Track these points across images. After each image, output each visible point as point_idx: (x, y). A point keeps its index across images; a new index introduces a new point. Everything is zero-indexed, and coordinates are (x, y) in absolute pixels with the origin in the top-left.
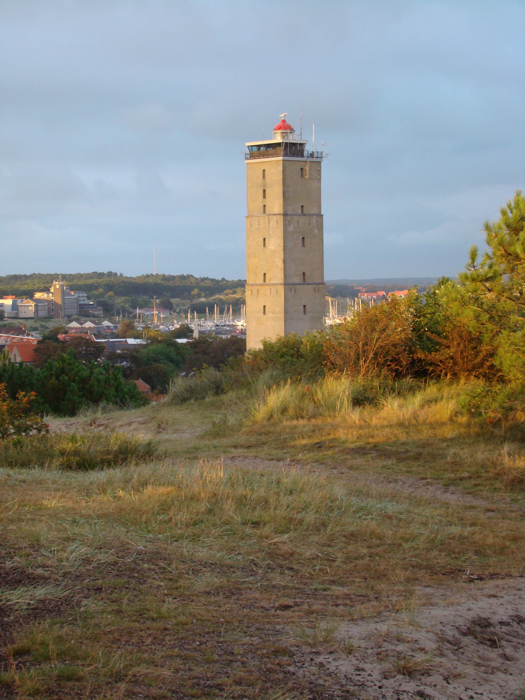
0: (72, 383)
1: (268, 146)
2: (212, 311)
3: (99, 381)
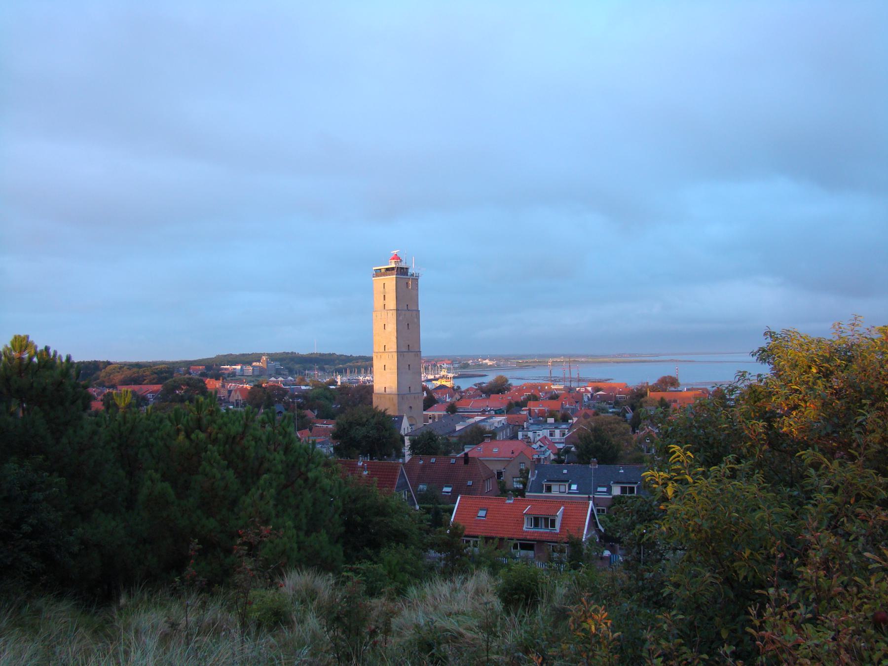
0: (210, 446)
1: (387, 269)
2: (346, 372)
3: (257, 439)
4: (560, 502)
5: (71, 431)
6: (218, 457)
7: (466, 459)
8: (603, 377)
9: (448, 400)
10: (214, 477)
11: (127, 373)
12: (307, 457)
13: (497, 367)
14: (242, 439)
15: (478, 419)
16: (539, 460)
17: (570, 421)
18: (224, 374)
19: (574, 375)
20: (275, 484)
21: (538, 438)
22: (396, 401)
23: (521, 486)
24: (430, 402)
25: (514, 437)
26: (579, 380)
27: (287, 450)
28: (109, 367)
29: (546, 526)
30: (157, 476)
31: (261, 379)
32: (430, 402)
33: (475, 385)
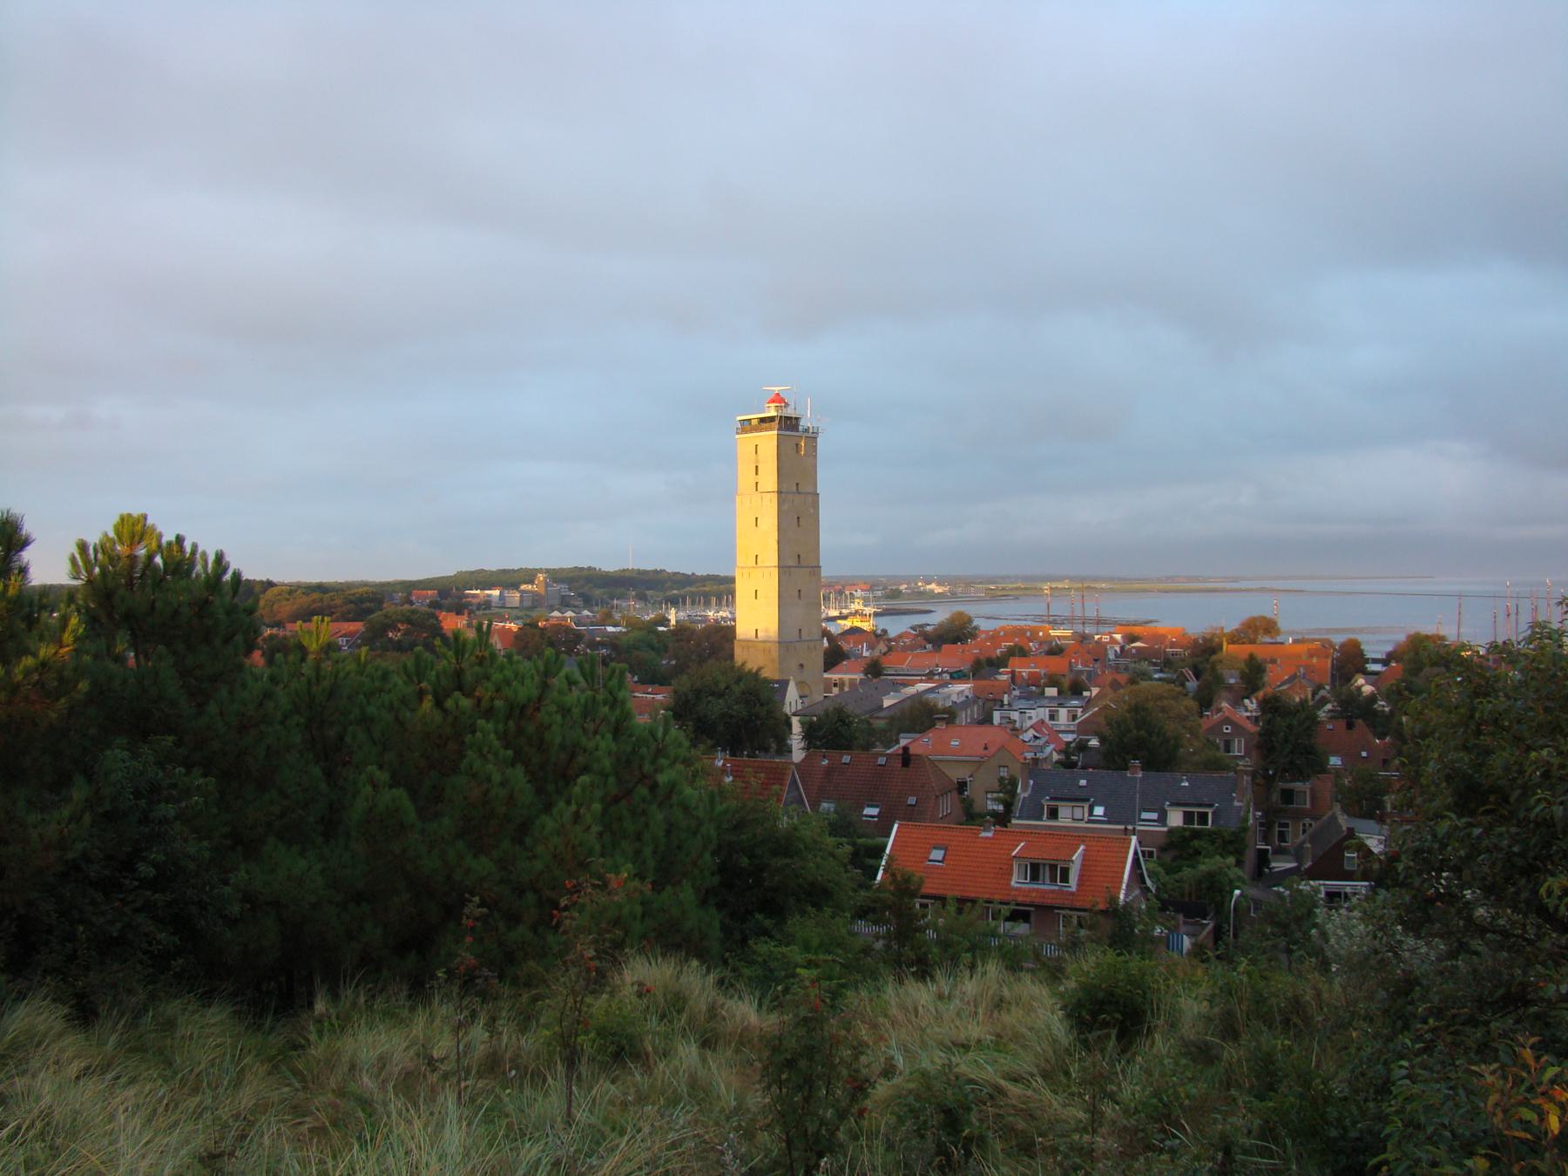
0: (481, 722)
1: (762, 420)
2: (684, 603)
3: (565, 711)
4: (1072, 837)
5: (224, 692)
6: (496, 743)
7: (906, 758)
8: (1141, 617)
9: (866, 654)
10: (489, 780)
11: (303, 601)
12: (653, 746)
13: (952, 597)
14: (538, 709)
15: (922, 687)
16: (1036, 761)
17: (1086, 694)
18: (470, 604)
19: (1091, 613)
20: (598, 793)
21: (1029, 723)
22: (775, 654)
23: (1001, 808)
24: (834, 657)
25: (987, 720)
26: (1099, 622)
27: (618, 731)
28: (271, 593)
29: (1053, 880)
30: (383, 777)
31: (534, 614)
32: (834, 657)
33: (913, 628)
